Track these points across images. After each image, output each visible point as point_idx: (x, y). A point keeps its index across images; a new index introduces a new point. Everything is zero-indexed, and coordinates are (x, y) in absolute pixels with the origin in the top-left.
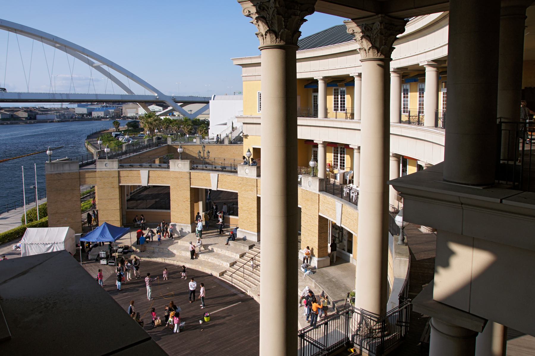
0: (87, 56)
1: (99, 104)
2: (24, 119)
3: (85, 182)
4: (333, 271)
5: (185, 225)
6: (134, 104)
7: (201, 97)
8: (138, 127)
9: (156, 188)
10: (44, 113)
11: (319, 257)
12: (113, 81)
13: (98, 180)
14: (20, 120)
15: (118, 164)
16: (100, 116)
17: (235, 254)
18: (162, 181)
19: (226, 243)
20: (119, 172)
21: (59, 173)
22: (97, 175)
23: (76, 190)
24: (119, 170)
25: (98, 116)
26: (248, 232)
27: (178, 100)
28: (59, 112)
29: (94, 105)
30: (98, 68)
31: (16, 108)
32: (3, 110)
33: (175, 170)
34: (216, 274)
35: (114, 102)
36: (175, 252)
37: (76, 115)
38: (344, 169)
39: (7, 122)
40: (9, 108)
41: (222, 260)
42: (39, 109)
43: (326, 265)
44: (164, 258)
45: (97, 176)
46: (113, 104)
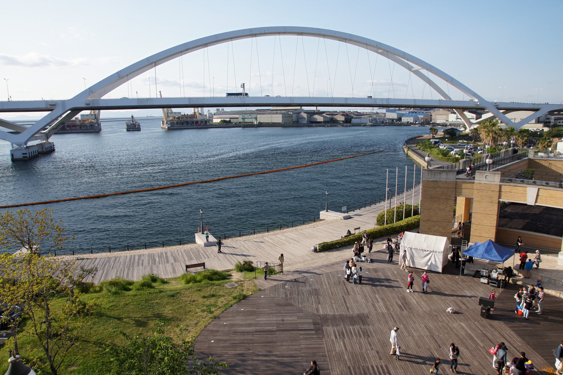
0: (407, 60)
1: (407, 109)
2: (341, 122)
3: (461, 192)
6: (445, 110)
7: (530, 104)
9: (518, 206)
10: (358, 117)
12: (432, 86)
13: (475, 192)
18: (556, 202)
20: (500, 186)
21: (435, 181)
22: (475, 186)
23: (450, 199)
24: (501, 184)
25: (407, 122)
29: (402, 110)
30: (417, 73)
31: (335, 112)
32: (325, 114)
39: (328, 124)
40: (329, 112)
44: (559, 292)
45: (475, 188)
46: (420, 110)
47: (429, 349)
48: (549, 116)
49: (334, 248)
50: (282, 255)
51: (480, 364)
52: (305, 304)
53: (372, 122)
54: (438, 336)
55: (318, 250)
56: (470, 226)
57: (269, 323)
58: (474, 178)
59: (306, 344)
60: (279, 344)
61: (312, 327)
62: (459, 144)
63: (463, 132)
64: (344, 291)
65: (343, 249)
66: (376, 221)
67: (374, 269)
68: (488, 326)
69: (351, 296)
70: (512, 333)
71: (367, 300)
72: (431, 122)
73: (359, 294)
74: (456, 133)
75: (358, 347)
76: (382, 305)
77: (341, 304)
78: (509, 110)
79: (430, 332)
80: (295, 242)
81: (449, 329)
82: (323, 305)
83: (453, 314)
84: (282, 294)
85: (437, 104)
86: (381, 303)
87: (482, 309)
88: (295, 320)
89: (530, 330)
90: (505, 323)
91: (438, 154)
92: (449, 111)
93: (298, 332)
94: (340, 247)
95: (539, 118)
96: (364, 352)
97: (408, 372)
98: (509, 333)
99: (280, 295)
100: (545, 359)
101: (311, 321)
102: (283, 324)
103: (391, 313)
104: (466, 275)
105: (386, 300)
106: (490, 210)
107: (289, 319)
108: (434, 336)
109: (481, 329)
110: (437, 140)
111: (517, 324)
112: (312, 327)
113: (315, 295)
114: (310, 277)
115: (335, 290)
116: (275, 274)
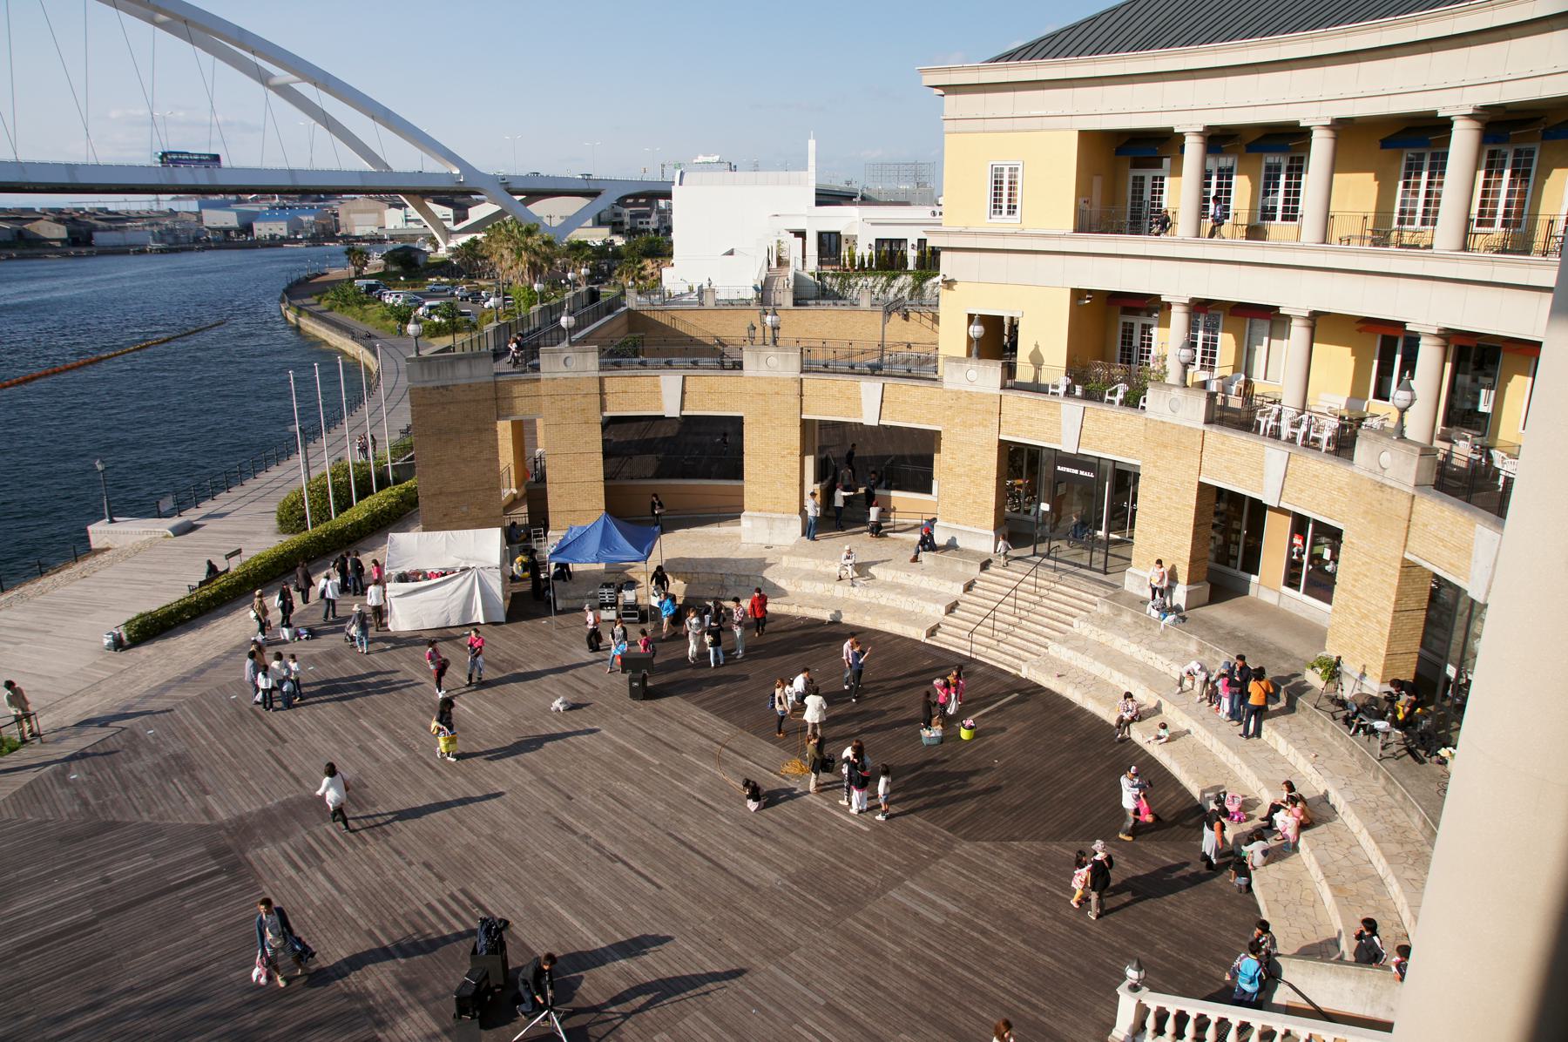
0: (253, 53)
1: (262, 199)
2: (58, 244)
4: (1221, 613)
5: (784, 516)
6: (371, 198)
8: (416, 265)
9: (625, 425)
10: (113, 225)
11: (1189, 583)
13: (546, 402)
14: (44, 247)
15: (597, 361)
16: (275, 235)
17: (949, 584)
19: (912, 557)
20: (601, 380)
21: (442, 387)
22: (543, 388)
25: (270, 235)
26: (967, 528)
27: (515, 186)
28: (157, 224)
29: (246, 201)
30: (285, 91)
31: (24, 210)
33: (758, 374)
34: (919, 634)
35: (305, 193)
36: (782, 583)
37: (207, 232)
38: (1212, 369)
39: (8, 252)
41: (920, 599)
42: (94, 214)
43: (1201, 603)
45: (543, 393)
46: (301, 200)
47: (548, 813)
48: (619, 209)
49: (177, 625)
50: (10, 685)
51: (668, 804)
52: (161, 808)
53: (162, 241)
54: (556, 773)
55: (127, 643)
56: (545, 490)
57: (63, 904)
58: (536, 368)
59: (214, 921)
60: (126, 952)
61: (211, 866)
62: (431, 287)
63: (432, 255)
64: (265, 735)
65: (207, 622)
66: (275, 523)
67: (325, 652)
68: (654, 716)
69: (293, 743)
70: (705, 714)
71: (340, 742)
72: (339, 234)
73: (312, 731)
74: (416, 258)
75: (370, 872)
76: (388, 742)
77: (271, 775)
78: (534, 195)
79: (533, 772)
80: (34, 636)
81: (573, 750)
82: (220, 794)
83: (567, 713)
84: (65, 802)
85: (356, 183)
86: (383, 739)
87: (631, 680)
88: (147, 866)
89: (735, 697)
90: (683, 698)
91: (385, 318)
92: (382, 200)
93: (172, 896)
94: (193, 617)
95: (599, 215)
96: (392, 877)
97: (521, 883)
98: (700, 716)
99: (60, 807)
100: (780, 747)
101: (202, 849)
102: (111, 890)
103: (420, 757)
104: (563, 612)
105: (392, 726)
106: (586, 442)
107: (122, 869)
108: (547, 777)
109: (640, 726)
110: (373, 282)
111: (707, 692)
112: (211, 865)
113: (183, 773)
114: (141, 727)
115: (239, 739)
116: (12, 750)
